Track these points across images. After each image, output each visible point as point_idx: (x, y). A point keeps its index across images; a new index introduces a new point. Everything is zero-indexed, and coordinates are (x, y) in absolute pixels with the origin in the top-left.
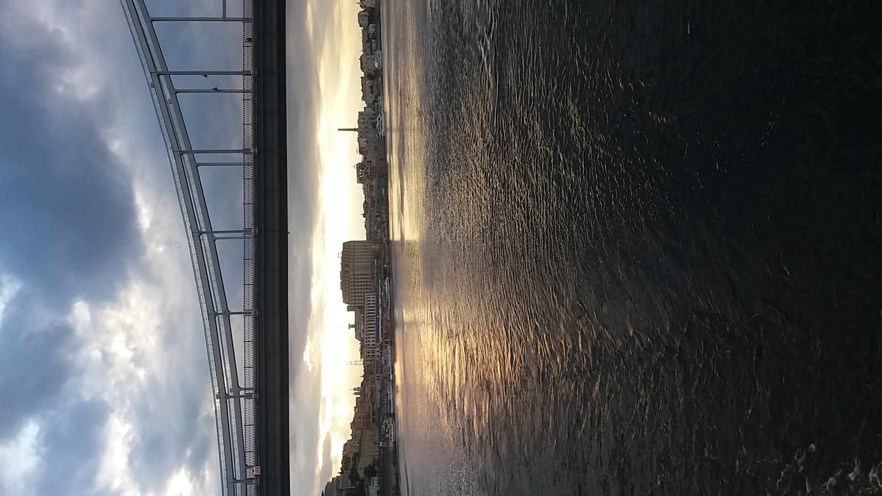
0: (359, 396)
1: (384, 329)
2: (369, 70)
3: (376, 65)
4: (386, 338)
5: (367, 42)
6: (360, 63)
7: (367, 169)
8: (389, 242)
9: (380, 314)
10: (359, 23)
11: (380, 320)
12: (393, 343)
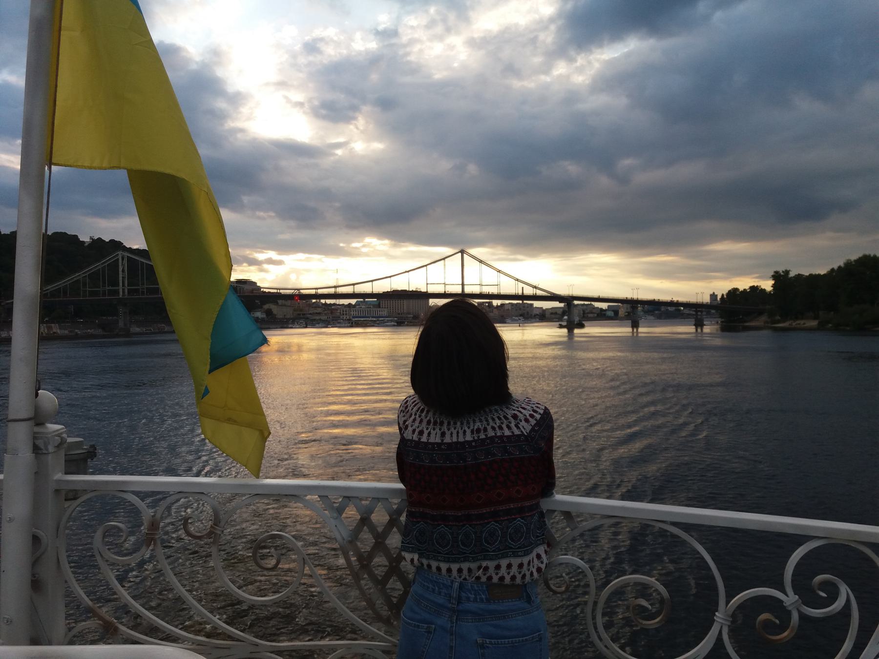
4: (355, 323)
11: (368, 319)
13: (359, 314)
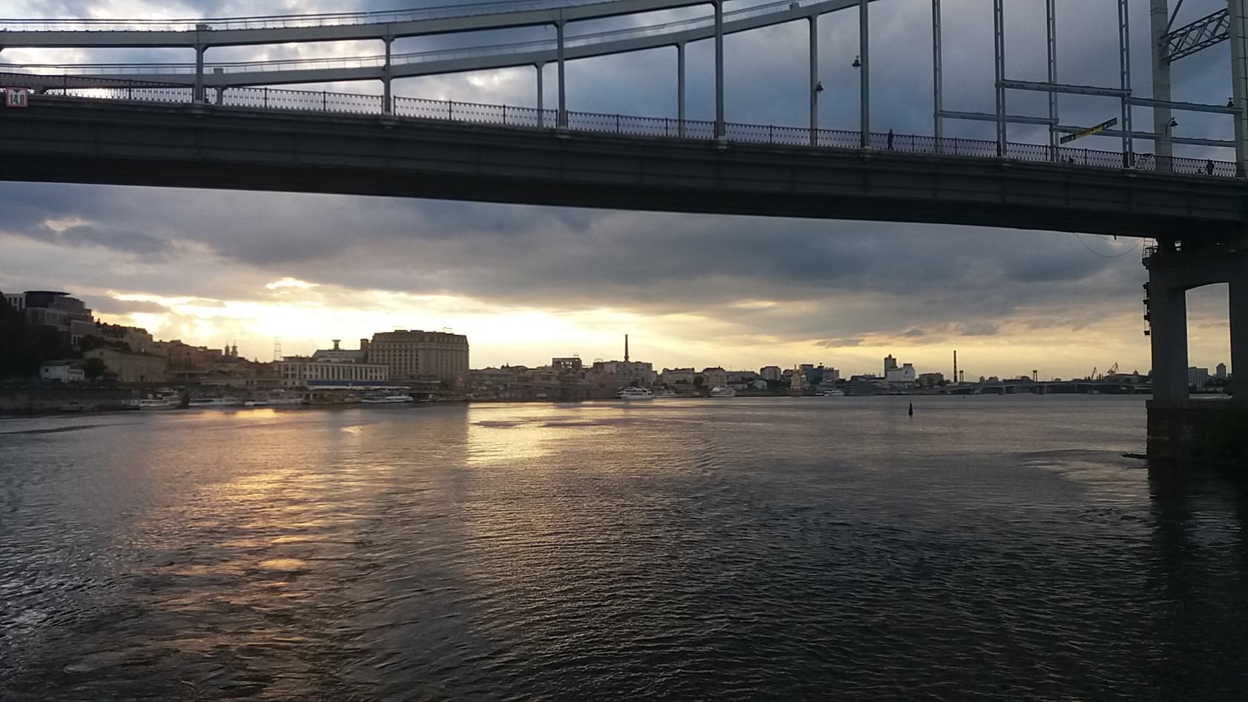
0: (223, 353)
1: (330, 393)
2: (708, 379)
3: (716, 389)
4: (314, 395)
5: (743, 378)
6: (713, 367)
7: (573, 373)
8: (468, 401)
9: (355, 387)
10: (766, 367)
11: (345, 387)
12: (306, 406)
13: (354, 377)
